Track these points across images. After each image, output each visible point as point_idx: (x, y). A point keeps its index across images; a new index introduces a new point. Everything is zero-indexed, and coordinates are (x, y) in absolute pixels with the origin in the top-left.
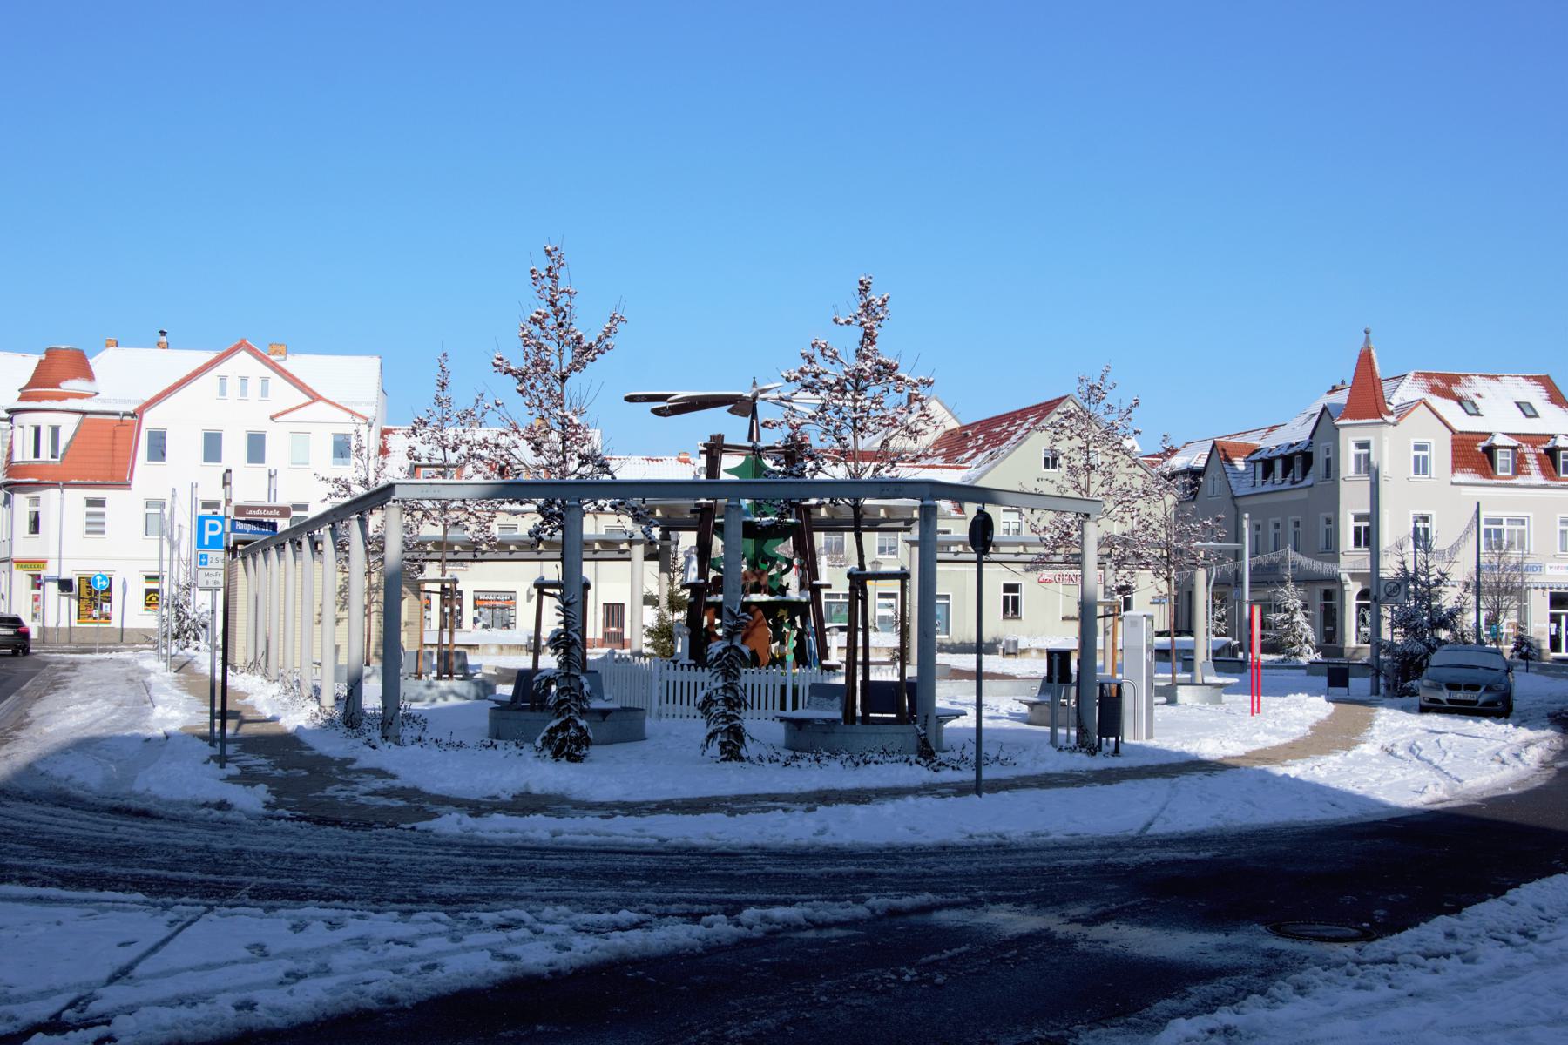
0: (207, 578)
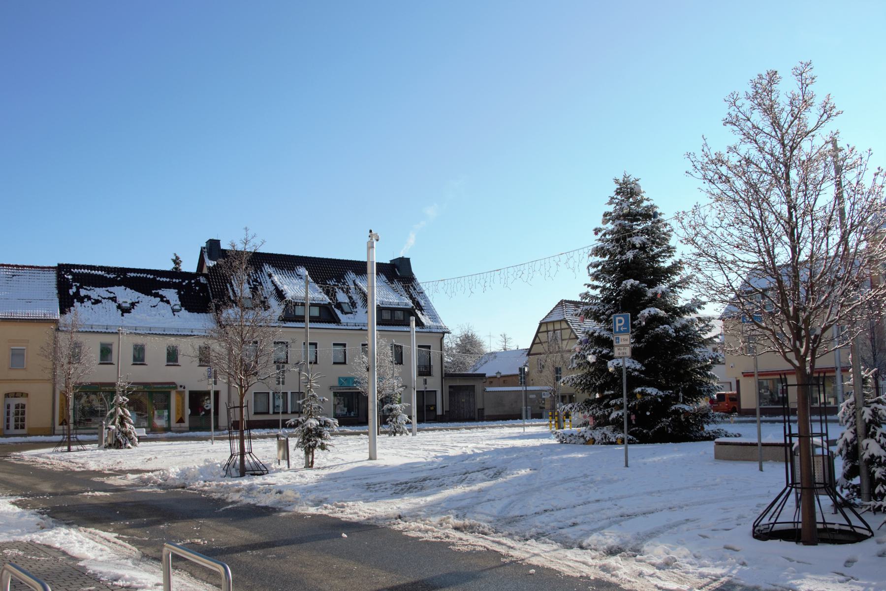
0: (619, 351)
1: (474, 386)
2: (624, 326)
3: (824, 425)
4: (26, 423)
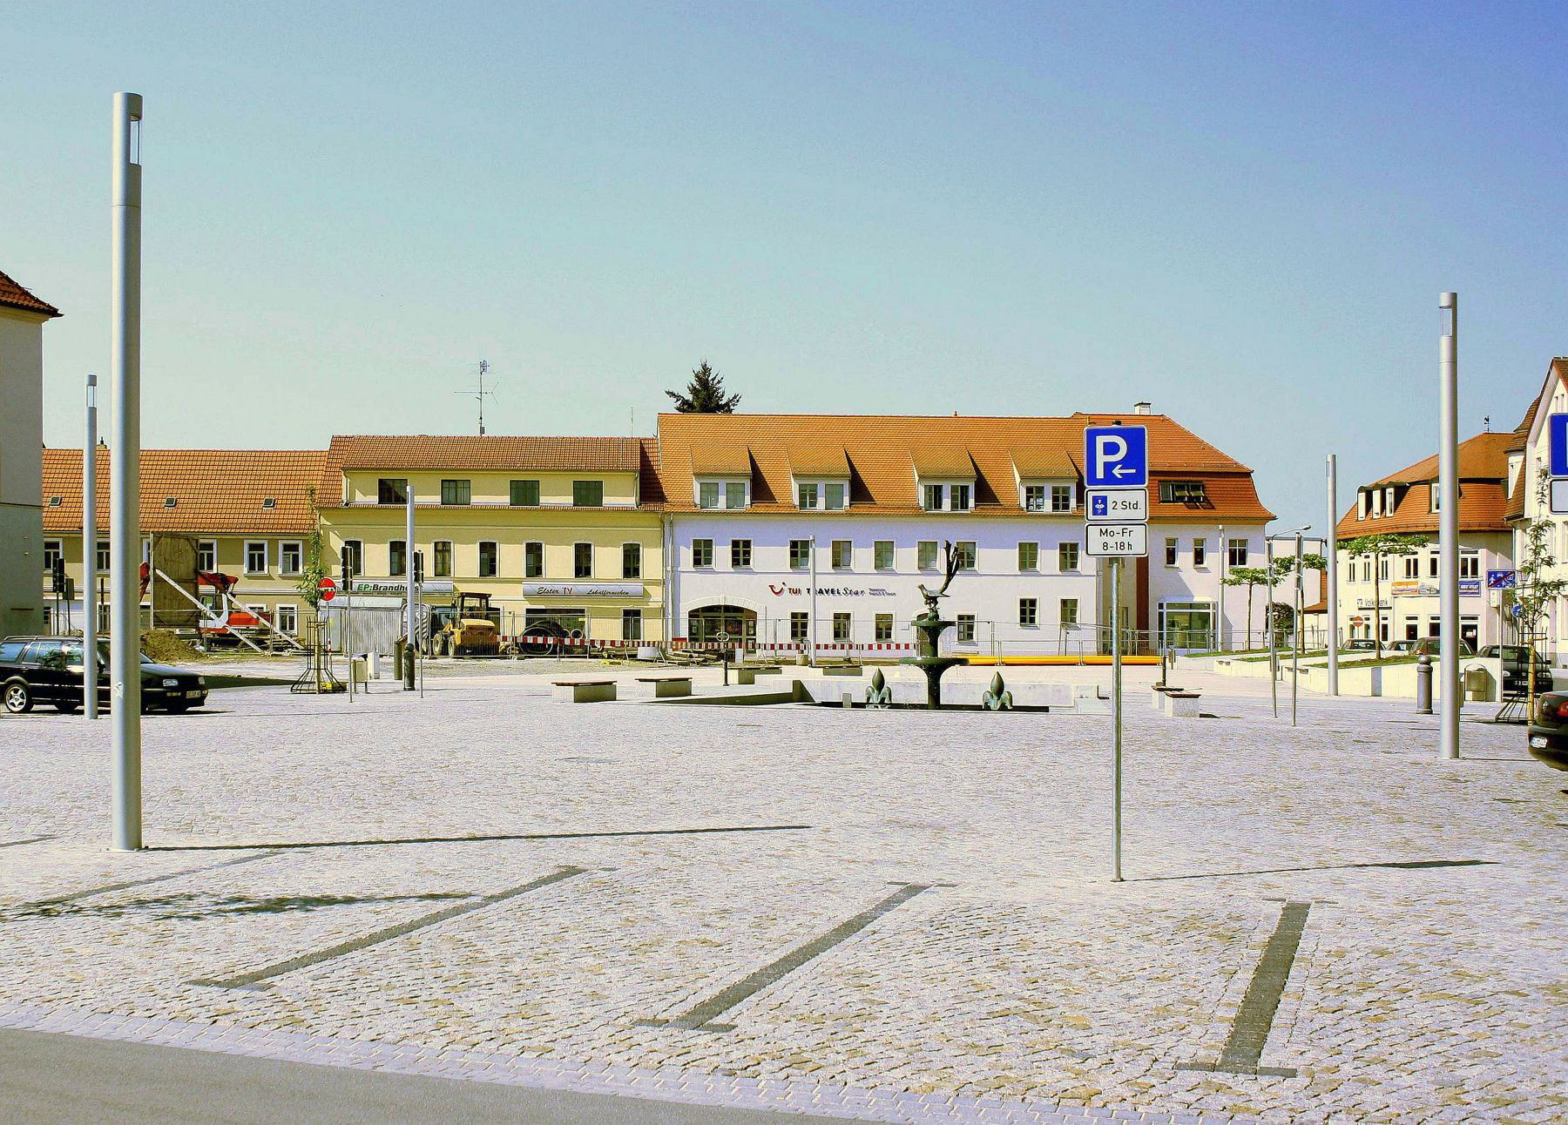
0: (1105, 538)
2: (1125, 463)
4: (788, 549)
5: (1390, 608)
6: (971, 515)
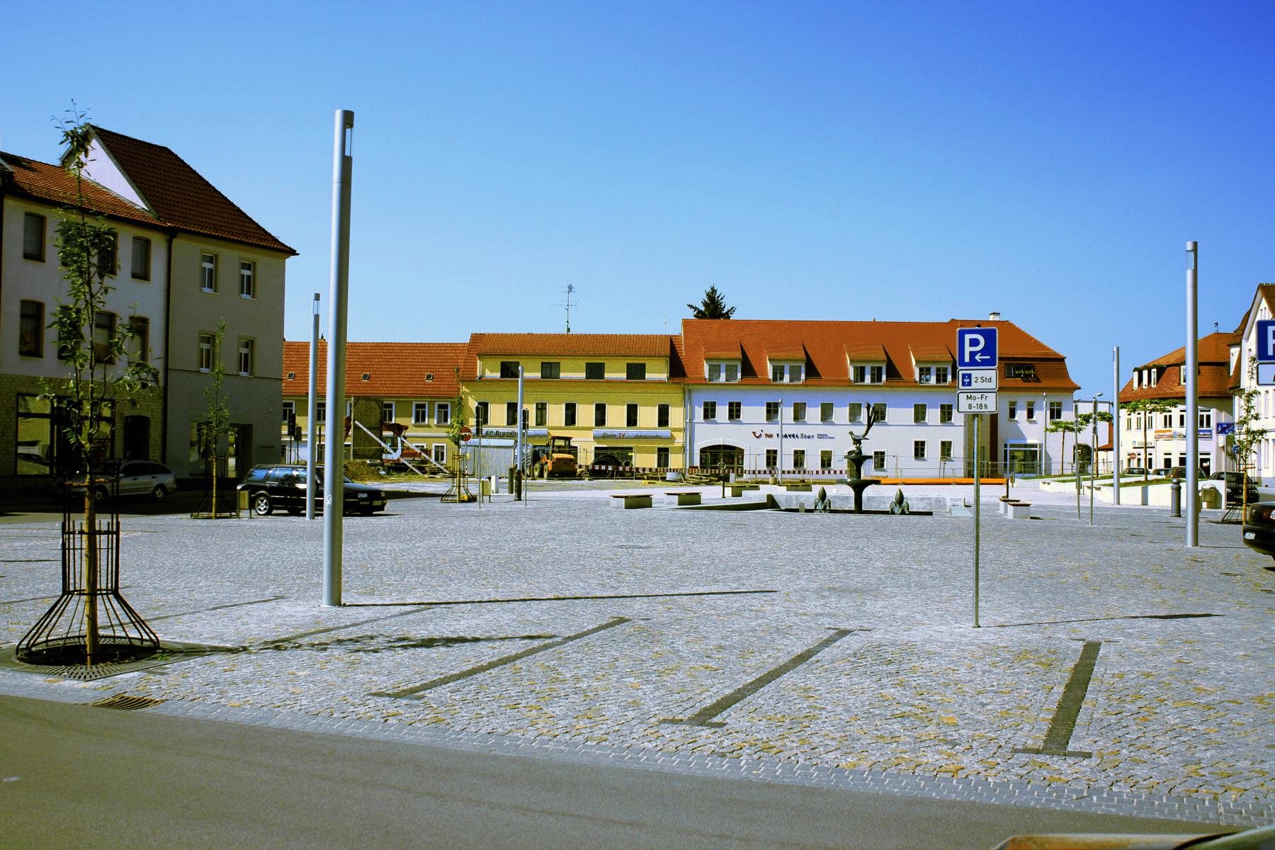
0: (970, 401)
1: (559, 363)
3: (942, 475)
5: (1154, 447)
6: (884, 386)
